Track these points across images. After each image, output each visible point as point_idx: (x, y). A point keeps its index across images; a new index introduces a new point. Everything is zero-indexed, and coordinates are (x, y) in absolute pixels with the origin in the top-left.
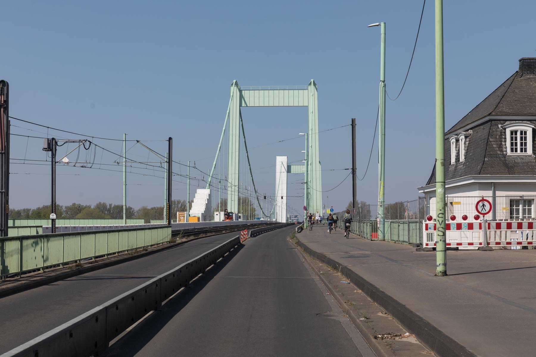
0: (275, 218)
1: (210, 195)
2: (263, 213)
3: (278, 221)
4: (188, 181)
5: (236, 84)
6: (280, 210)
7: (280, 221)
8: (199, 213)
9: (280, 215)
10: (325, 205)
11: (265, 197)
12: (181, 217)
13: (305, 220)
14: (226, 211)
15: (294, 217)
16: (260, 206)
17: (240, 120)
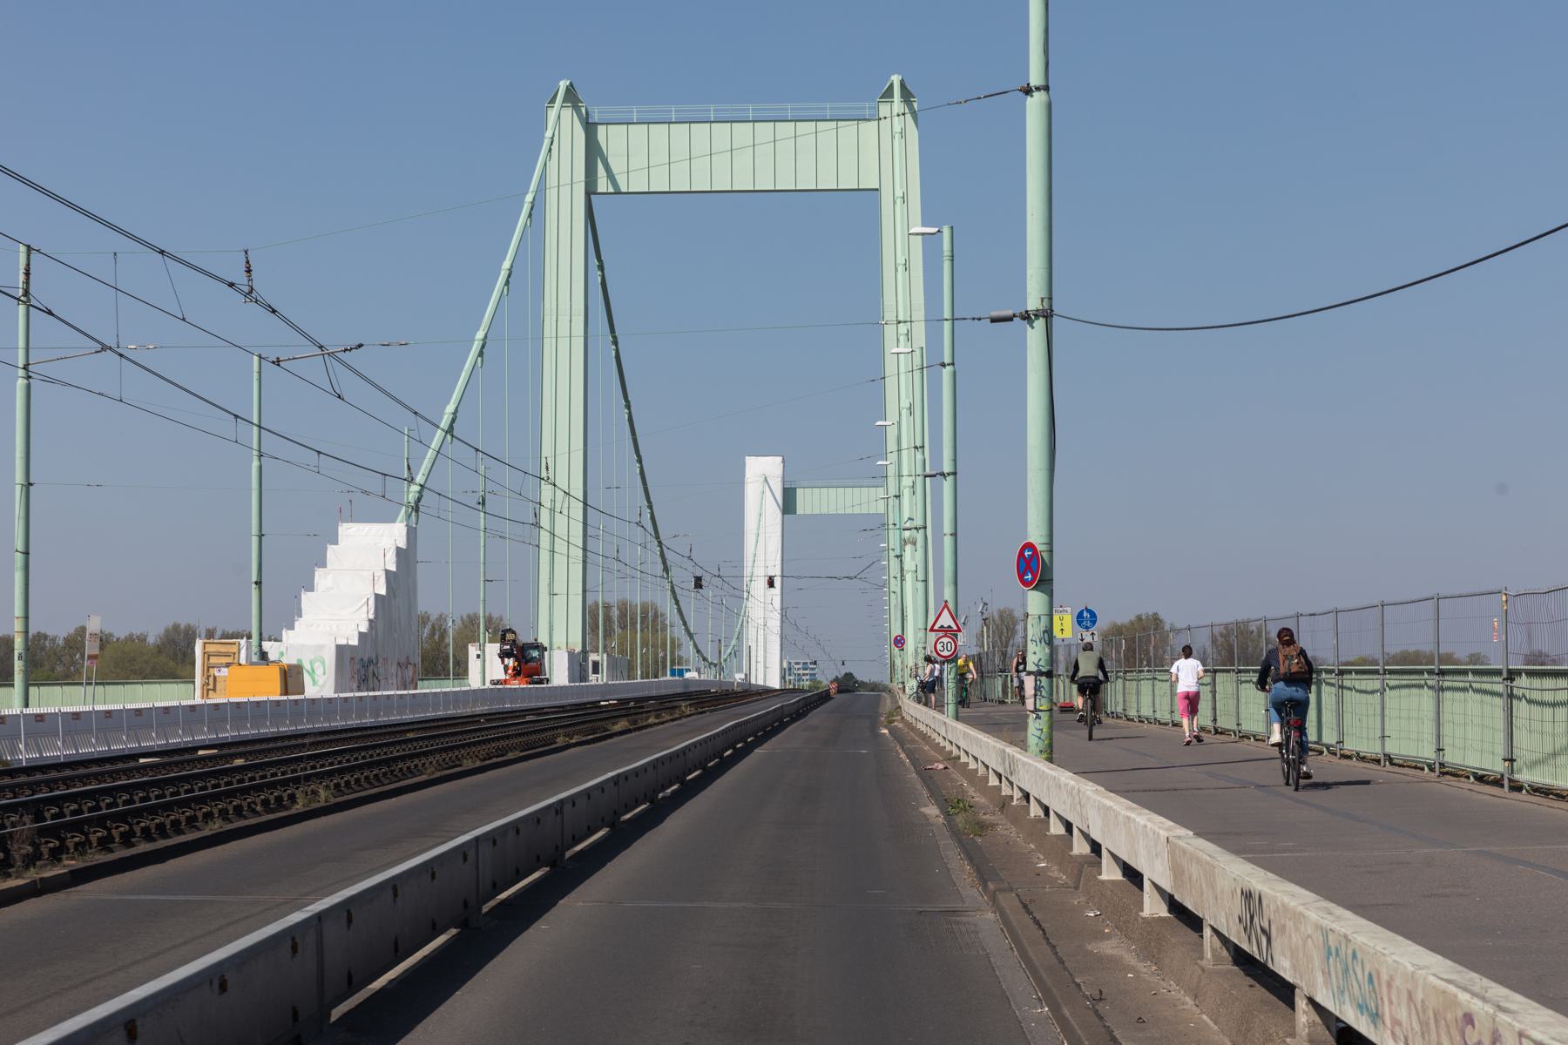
0: (740, 671)
1: (405, 556)
2: (698, 651)
3: (753, 682)
4: (255, 464)
5: (571, 97)
6: (761, 639)
7: (761, 682)
8: (321, 647)
9: (761, 659)
10: (985, 604)
11: (698, 583)
12: (219, 666)
13: (1037, 689)
14: (509, 636)
15: (800, 666)
16: (685, 624)
17: (594, 262)
